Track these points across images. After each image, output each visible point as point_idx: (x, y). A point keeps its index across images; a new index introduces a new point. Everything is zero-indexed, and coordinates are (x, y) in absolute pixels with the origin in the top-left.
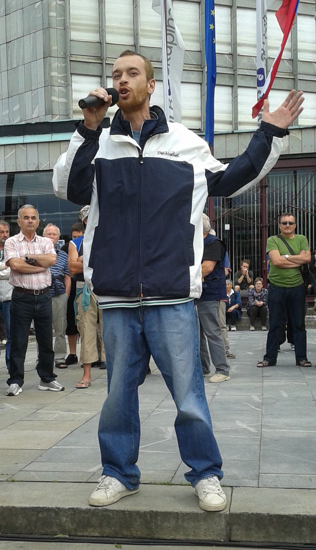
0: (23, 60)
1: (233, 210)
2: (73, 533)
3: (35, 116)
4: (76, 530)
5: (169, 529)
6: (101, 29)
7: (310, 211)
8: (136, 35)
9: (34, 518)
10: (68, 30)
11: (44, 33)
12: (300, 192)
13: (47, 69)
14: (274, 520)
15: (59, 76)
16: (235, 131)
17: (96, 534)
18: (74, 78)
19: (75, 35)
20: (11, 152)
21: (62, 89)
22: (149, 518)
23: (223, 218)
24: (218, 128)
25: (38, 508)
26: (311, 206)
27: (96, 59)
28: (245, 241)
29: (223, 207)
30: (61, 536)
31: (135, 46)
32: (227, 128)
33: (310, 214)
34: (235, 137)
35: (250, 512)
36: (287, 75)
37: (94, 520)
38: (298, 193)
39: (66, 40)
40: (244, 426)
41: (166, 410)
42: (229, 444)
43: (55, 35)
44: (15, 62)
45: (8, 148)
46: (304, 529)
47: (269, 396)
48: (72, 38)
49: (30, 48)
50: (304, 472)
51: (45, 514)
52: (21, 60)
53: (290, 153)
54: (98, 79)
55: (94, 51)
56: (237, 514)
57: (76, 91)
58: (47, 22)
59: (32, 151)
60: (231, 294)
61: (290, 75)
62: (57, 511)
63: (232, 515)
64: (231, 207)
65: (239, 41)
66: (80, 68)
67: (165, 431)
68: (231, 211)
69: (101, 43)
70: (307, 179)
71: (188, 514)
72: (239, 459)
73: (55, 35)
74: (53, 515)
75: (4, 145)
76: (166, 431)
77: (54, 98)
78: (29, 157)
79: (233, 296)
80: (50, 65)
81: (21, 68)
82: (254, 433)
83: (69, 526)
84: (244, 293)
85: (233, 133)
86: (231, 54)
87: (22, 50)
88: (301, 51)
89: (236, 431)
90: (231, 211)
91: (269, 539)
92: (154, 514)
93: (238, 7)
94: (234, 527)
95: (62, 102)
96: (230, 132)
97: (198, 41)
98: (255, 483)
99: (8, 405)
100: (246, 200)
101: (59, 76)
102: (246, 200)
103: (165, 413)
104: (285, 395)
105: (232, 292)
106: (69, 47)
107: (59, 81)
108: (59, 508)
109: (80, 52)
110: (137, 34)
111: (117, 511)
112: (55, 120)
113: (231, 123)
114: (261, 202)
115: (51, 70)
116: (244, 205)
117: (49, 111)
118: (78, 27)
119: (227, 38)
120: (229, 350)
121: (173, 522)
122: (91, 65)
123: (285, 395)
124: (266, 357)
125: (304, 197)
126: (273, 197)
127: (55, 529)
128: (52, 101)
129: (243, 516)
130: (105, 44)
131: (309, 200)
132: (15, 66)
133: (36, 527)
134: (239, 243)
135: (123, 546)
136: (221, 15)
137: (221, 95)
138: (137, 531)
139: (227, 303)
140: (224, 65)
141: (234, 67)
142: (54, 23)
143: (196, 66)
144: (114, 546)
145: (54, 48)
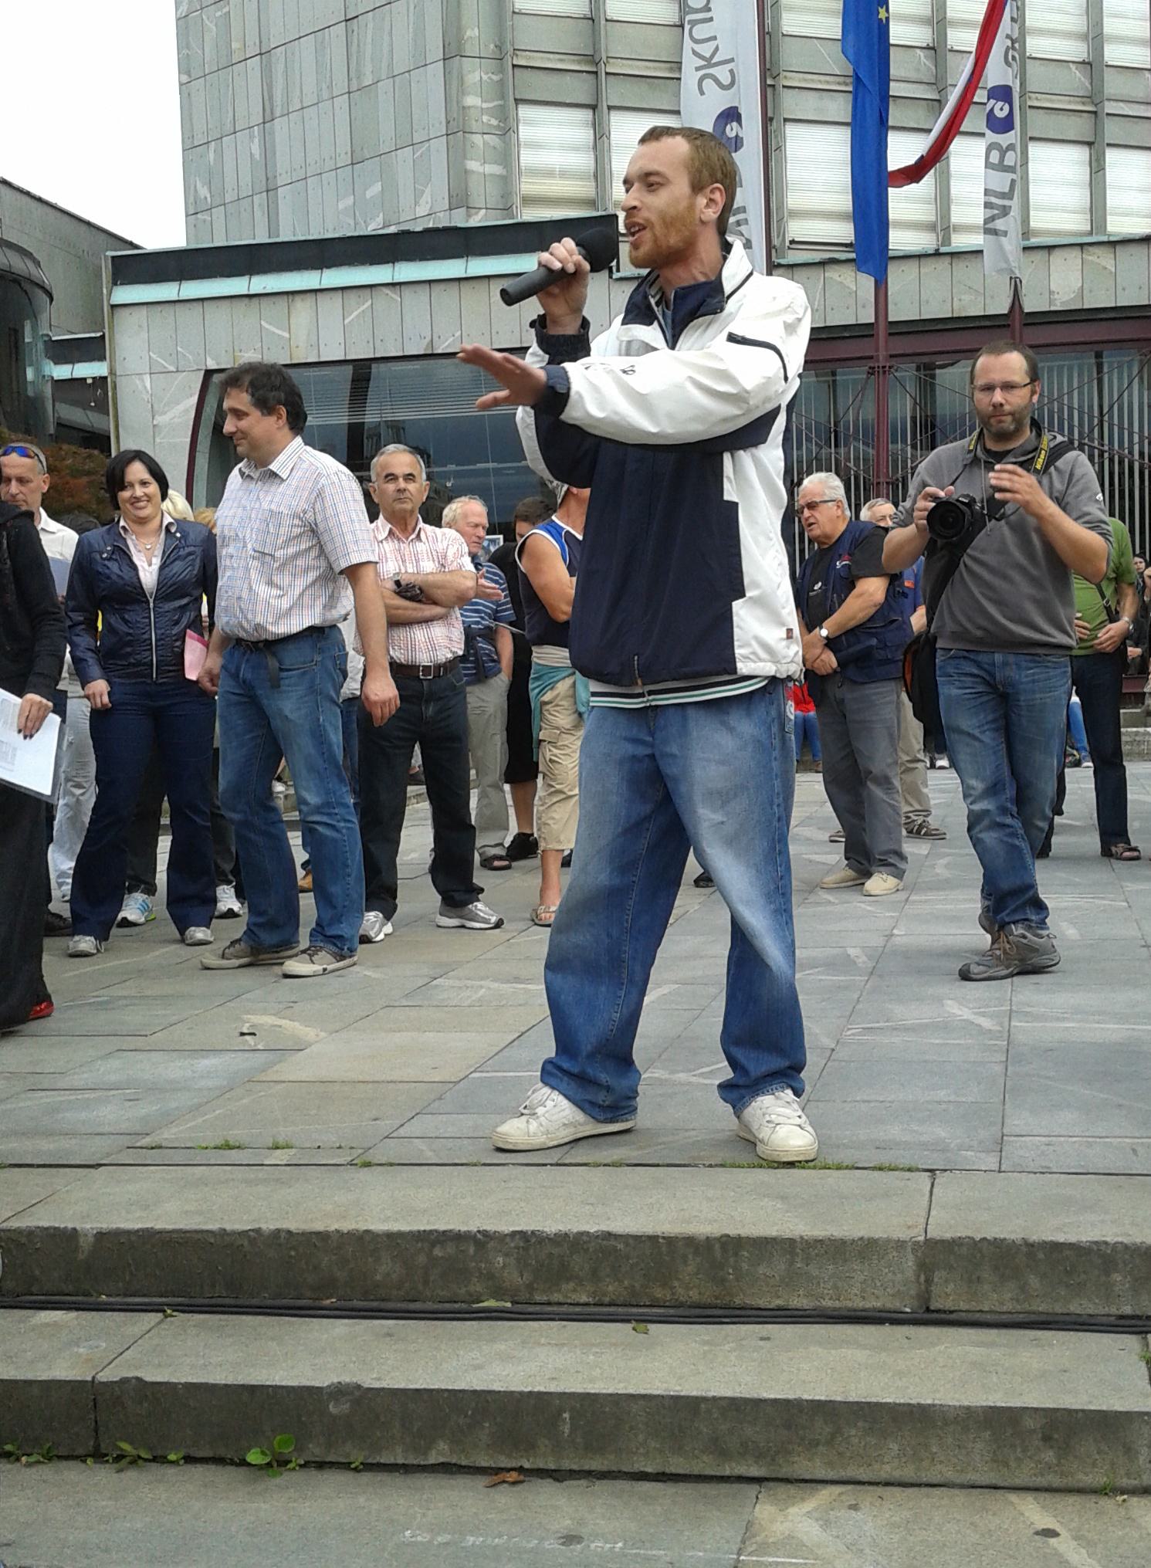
0: (390, 66)
2: (524, 1296)
3: (421, 211)
4: (530, 1287)
7: (1136, 456)
12: (1111, 407)
13: (453, 87)
14: (1041, 1256)
15: (485, 105)
16: (943, 250)
17: (584, 1299)
18: (525, 111)
20: (360, 307)
24: (899, 240)
26: (1141, 443)
27: (579, 62)
30: (491, 1303)
32: (922, 241)
34: (943, 264)
35: (978, 1237)
37: (578, 1263)
40: (966, 1014)
45: (352, 296)
46: (1117, 1277)
52: (384, 65)
54: (586, 115)
62: (483, 1240)
71: (819, 1242)
74: (472, 1250)
77: (473, 165)
81: (385, 86)
83: (514, 1278)
86: (933, 48)
87: (386, 38)
88: (796, 214)
91: (1026, 1307)
92: (732, 1245)
98: (991, 1162)
101: (485, 105)
107: (485, 118)
108: (485, 1233)
112: (476, 221)
115: (462, 91)
117: (459, 199)
121: (778, 1267)
122: (568, 77)
127: (477, 1287)
128: (466, 171)
130: (603, 22)
133: (426, 1283)
135: (652, 1327)
138: (688, 1288)
140: (913, 76)
143: (841, 79)
145: (471, 33)
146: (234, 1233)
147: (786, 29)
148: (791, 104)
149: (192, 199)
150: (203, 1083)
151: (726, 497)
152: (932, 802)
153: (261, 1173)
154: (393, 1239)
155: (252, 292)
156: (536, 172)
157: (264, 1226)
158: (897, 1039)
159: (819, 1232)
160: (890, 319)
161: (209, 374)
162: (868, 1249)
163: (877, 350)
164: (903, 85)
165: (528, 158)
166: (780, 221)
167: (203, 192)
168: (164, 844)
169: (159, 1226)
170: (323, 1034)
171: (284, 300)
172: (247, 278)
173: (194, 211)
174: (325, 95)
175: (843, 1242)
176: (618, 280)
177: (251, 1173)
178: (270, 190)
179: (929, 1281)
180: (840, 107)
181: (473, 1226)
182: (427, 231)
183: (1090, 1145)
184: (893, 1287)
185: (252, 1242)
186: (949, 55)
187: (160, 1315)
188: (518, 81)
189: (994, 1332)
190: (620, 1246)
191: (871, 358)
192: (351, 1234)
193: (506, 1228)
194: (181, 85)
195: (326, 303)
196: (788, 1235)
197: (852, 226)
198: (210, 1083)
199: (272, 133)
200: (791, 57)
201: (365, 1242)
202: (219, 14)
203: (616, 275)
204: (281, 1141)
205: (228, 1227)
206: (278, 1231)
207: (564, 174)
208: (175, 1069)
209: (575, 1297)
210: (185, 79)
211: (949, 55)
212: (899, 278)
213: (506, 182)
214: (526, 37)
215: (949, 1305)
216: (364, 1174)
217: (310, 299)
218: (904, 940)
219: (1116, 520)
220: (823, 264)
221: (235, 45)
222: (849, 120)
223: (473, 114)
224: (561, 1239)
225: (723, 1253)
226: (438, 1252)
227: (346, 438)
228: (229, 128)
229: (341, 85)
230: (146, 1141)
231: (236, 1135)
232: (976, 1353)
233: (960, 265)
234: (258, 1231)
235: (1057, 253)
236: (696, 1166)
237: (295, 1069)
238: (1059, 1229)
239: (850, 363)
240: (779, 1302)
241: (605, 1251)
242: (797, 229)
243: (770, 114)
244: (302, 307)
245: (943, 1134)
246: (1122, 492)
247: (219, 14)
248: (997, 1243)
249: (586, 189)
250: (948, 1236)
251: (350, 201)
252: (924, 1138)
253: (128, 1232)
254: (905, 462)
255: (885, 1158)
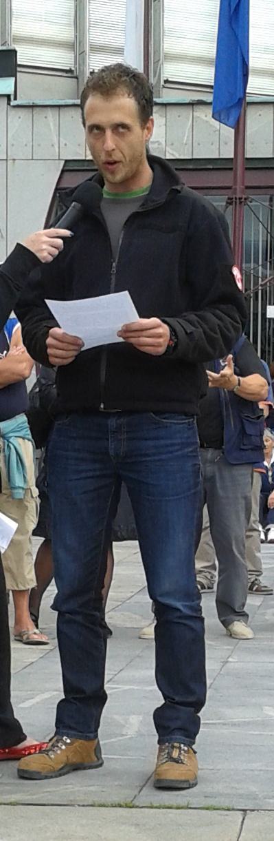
42: (247, 745)
67: (123, 722)
72: (263, 768)
76: (126, 723)
88: (171, 57)
103: (125, 691)
113: (71, 46)
120: (260, 578)
151: (127, 292)
152: (264, 566)
160: (248, 156)
163: (235, 183)
176: (14, 107)
191: (229, 188)
197: (213, 70)
203: (13, 103)
218: (236, 665)
236: (73, 805)
239: (214, 192)
242: (171, 71)
245: (254, 789)
252: (241, 792)
254: (256, 277)
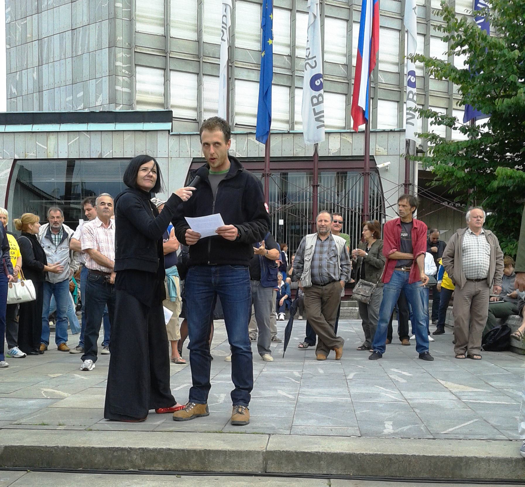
0: (88, 48)
1: (288, 206)
2: (142, 468)
3: (98, 104)
4: (144, 465)
5: (219, 464)
6: (166, 23)
7: (357, 211)
8: (199, 31)
9: (110, 456)
10: (134, 22)
11: (110, 23)
12: (349, 192)
13: (112, 58)
14: (300, 456)
15: (124, 66)
16: (291, 132)
17: (161, 469)
18: (138, 69)
19: (140, 27)
20: (75, 139)
21: (126, 79)
22: (203, 455)
23: (278, 214)
24: (275, 126)
25: (113, 448)
26: (359, 205)
27: (160, 52)
28: (297, 236)
29: (278, 203)
30: (132, 470)
31: (198, 41)
32: (285, 127)
33: (357, 214)
34: (290, 137)
35: (281, 450)
36: (341, 79)
37: (159, 458)
38: (347, 192)
39: (131, 32)
40: (284, 394)
41: (219, 382)
43: (121, 24)
44: (80, 48)
45: (71, 135)
46: (322, 462)
47: (308, 372)
48: (137, 30)
49: (95, 36)
50: (327, 425)
51: (119, 453)
52: (86, 47)
53: (341, 155)
54: (162, 72)
55: (158, 44)
56: (271, 452)
57: (140, 82)
58: (113, 12)
59: (96, 139)
60: (282, 285)
61: (344, 80)
62: (130, 450)
63: (267, 452)
64: (285, 203)
65: (297, 44)
66: (145, 60)
68: (285, 207)
69: (165, 37)
70: (356, 179)
71: (234, 452)
73: (121, 24)
74: (126, 453)
75: (68, 132)
77: (118, 88)
78: (92, 144)
79: (284, 287)
80: (115, 55)
81: (86, 56)
82: (291, 399)
83: (139, 462)
84: (294, 285)
85: (289, 133)
86: (290, 56)
87: (87, 38)
88: (237, 114)
89: (278, 398)
90: (285, 207)
91: (295, 471)
92: (207, 452)
93: (298, 11)
94: (269, 461)
95: (125, 92)
96: (286, 132)
97: (258, 41)
98: (288, 432)
99: (78, 376)
100: (299, 197)
101: (124, 66)
102: (299, 197)
103: (218, 383)
104: (321, 371)
105: (283, 283)
106: (134, 38)
107: (124, 71)
108: (130, 448)
109: (145, 44)
110: (201, 30)
111: (178, 450)
112: (118, 110)
114: (313, 200)
115: (115, 60)
116: (297, 202)
117: (113, 100)
118: (143, 19)
119: (287, 40)
121: (222, 458)
122: (155, 57)
123: (321, 371)
124: (306, 340)
125: (352, 197)
126: (324, 196)
127: (127, 465)
128: (116, 90)
129: (276, 453)
130: (169, 38)
131: (357, 201)
132: (80, 53)
133: (111, 463)
134: (292, 237)
135: (182, 476)
136: (280, 18)
137: (279, 95)
138: (193, 466)
139: (278, 292)
140: (283, 66)
141: (292, 69)
142: (120, 14)
143: (256, 65)
144: (175, 476)
145: (120, 38)
146: (49, 447)
147: (236, 45)
148: (239, 73)
149: (9, 93)
150: (31, 407)
153: (56, 432)
154: (101, 450)
155: (33, 131)
156: (141, 92)
157: (60, 445)
158: (261, 400)
159: (234, 449)
160: (271, 156)
161: (15, 160)
162: (249, 454)
163: (266, 167)
164: (279, 69)
165: (139, 86)
166: (232, 116)
167: (14, 90)
168: (209, 250)
169: (25, 445)
170: (70, 395)
171: (12, 134)
172: (31, 125)
173: (10, 97)
174: (63, 57)
175: (241, 452)
177: (53, 432)
178: (40, 91)
179: (266, 464)
180: (255, 76)
181: (127, 446)
182: (101, 112)
183: (318, 428)
184: (256, 466)
185: (56, 450)
186: (296, 59)
187: (26, 472)
188: (136, 58)
189: (285, 478)
190: (173, 453)
191: (263, 170)
192: (87, 448)
193: (137, 447)
194: (7, 49)
195: (61, 137)
196: (224, 449)
198: (34, 407)
199: (42, 70)
200: (238, 56)
201: (92, 450)
202: (22, 23)
203: (171, 133)
204: (61, 423)
205: (48, 445)
206: (64, 447)
207: (152, 94)
208: (21, 403)
209: (158, 468)
210: (8, 47)
211: (296, 59)
212: (274, 142)
213: (131, 95)
214: (141, 41)
215: (272, 471)
216: (89, 432)
217: (55, 135)
218: (266, 373)
219: (346, 234)
220: (247, 134)
221: (28, 36)
222: (259, 80)
223: (119, 69)
224: (155, 450)
225: (205, 455)
226: (115, 454)
227: (65, 188)
228: (25, 66)
229: (69, 53)
230: (16, 422)
231: (46, 421)
232: (279, 483)
233: (297, 138)
234: (58, 447)
235: (331, 135)
237: (61, 404)
238: (306, 449)
240: (221, 470)
241: (168, 454)
243: (230, 77)
244: (52, 138)
246: (352, 223)
247: (22, 23)
248: (287, 452)
249: (161, 100)
250: (272, 450)
251: (71, 98)
252: (268, 426)
253: (15, 446)
255: (255, 431)
